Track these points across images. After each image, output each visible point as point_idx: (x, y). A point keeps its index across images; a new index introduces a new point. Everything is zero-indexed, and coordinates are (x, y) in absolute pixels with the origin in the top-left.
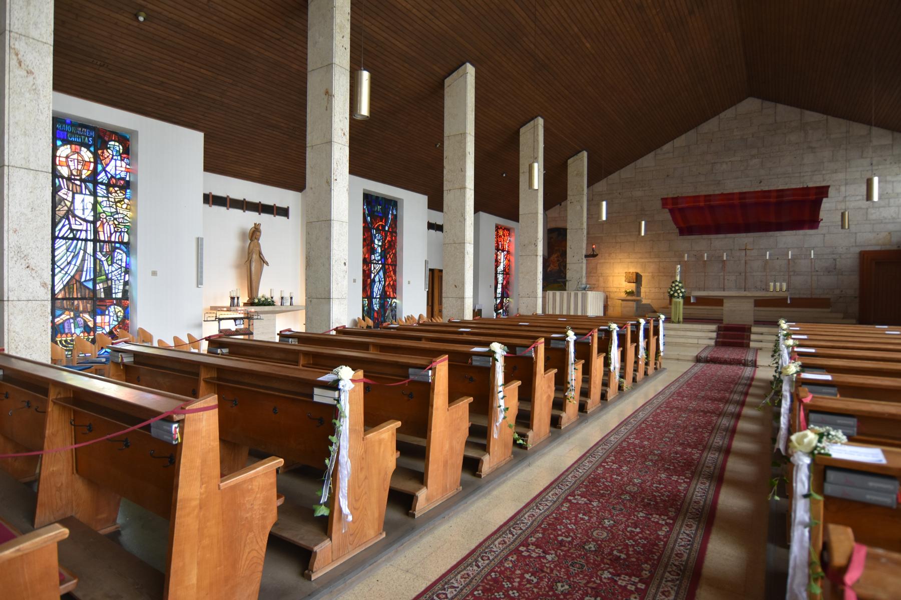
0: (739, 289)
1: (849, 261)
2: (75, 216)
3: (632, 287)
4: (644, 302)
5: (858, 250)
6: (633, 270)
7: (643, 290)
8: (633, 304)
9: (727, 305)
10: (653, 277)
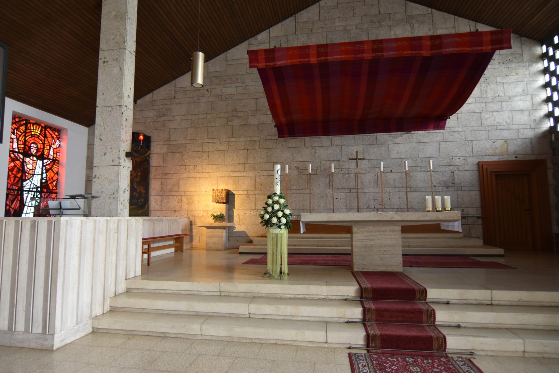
0: (349, 209)
1: (468, 174)
2: (52, 171)
3: (221, 209)
4: (238, 228)
5: (476, 161)
6: (223, 186)
7: (236, 213)
8: (224, 233)
9: (360, 237)
10: (248, 196)
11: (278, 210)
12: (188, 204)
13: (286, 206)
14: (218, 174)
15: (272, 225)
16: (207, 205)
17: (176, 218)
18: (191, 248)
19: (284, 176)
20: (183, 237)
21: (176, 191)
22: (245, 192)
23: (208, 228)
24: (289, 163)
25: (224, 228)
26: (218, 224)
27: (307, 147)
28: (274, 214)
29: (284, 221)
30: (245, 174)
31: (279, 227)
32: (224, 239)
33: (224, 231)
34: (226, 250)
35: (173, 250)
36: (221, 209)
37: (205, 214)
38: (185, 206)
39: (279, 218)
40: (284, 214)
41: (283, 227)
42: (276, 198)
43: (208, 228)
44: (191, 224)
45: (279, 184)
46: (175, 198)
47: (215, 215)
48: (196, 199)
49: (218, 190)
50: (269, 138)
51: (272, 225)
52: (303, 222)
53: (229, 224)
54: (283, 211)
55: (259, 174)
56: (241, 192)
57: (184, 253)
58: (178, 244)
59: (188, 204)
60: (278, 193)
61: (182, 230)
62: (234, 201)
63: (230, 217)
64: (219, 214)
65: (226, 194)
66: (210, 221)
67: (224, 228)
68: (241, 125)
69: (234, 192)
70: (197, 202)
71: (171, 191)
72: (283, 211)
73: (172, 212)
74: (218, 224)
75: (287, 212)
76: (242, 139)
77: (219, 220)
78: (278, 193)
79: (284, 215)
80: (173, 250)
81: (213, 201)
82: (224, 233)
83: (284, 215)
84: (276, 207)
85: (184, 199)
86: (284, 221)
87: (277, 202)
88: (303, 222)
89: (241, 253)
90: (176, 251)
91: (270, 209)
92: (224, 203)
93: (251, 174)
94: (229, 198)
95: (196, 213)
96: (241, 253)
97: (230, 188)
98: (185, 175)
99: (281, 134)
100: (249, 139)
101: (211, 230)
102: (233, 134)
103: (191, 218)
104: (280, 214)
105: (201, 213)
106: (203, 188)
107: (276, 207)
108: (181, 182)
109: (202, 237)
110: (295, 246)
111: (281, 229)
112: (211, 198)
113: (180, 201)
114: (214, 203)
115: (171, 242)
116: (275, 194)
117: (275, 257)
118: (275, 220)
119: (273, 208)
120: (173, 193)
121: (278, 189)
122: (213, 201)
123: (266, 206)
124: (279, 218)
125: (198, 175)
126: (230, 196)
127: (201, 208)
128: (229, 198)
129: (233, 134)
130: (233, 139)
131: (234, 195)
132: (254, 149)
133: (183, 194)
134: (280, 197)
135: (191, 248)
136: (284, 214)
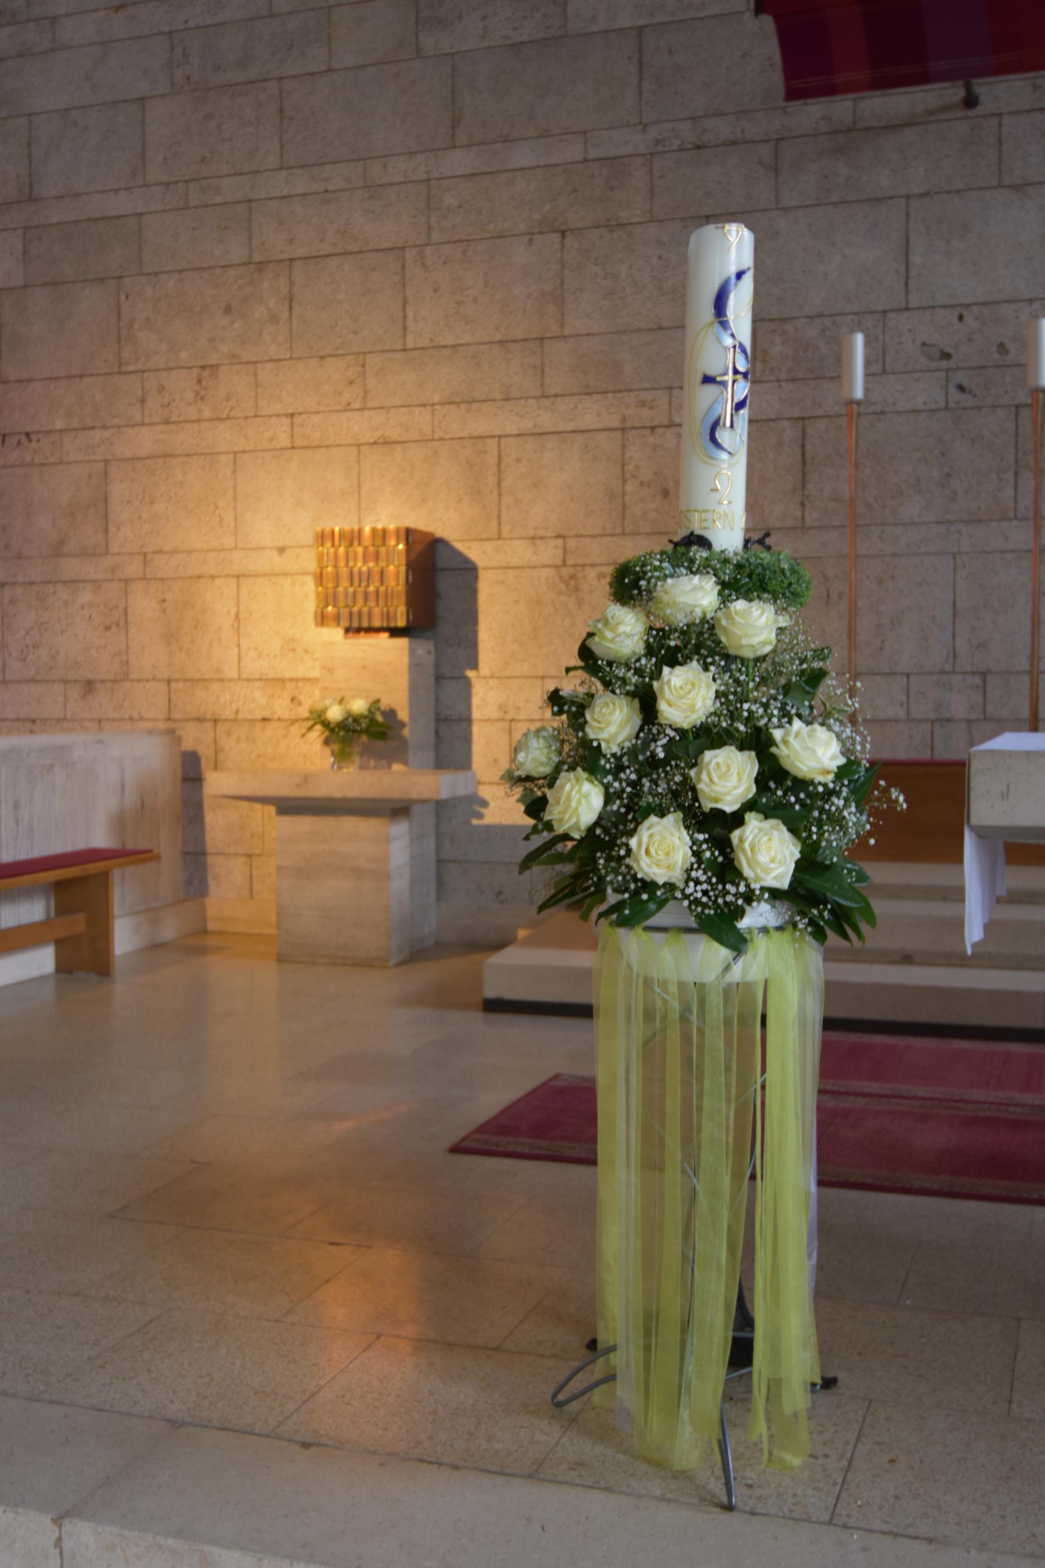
8: (397, 845)
11: (707, 736)
12: (170, 638)
13: (800, 685)
14: (361, 426)
15: (642, 900)
16: (291, 646)
17: (60, 739)
18: (199, 942)
19: (790, 350)
20: (104, 878)
21: (89, 554)
22: (550, 552)
23: (288, 807)
24: (877, 321)
25: (398, 810)
26: (355, 780)
27: (1019, 188)
28: (656, 773)
29: (770, 853)
30: (546, 420)
31: (721, 924)
32: (400, 885)
33: (400, 829)
34: (416, 954)
35: (41, 961)
36: (378, 670)
37: (282, 708)
38: (149, 654)
39: (716, 828)
40: (772, 774)
41: (758, 916)
42: (694, 595)
43: (288, 807)
44: (191, 772)
45: (736, 438)
46: (85, 596)
47: (335, 714)
48: (219, 600)
49: (353, 537)
50: (722, 129)
51: (642, 900)
52: (983, 834)
53: (440, 785)
54: (759, 743)
55: (645, 416)
56: (520, 552)
57: (122, 988)
58: (76, 924)
59: (170, 638)
60: (728, 534)
61: (119, 822)
62: (471, 617)
63: (448, 734)
64: (359, 706)
65: (412, 565)
66: (310, 761)
67: (398, 810)
68: (516, 47)
69: (474, 553)
70: (227, 622)
71: (58, 550)
72: (759, 743)
73: (75, 693)
74: (355, 780)
75: (815, 751)
76: (523, 156)
77: (366, 752)
78: (728, 534)
79: (779, 790)
80: (41, 961)
81: (322, 619)
82: (397, 845)
83: (779, 790)
84: (689, 695)
85: (143, 605)
86: (770, 853)
87: (700, 643)
88: (983, 834)
89: (495, 1006)
90: (64, 967)
91: (613, 723)
92: (395, 632)
93: (591, 413)
94: (433, 595)
95: (225, 701)
96: (495, 1006)
97: (445, 521)
98: (144, 440)
99: (808, 71)
100: (573, 152)
101: (305, 823)
102: (456, 122)
103: (192, 738)
104: (727, 777)
105: (256, 701)
106: (263, 530)
107: (689, 695)
108: (118, 490)
109: (257, 866)
110: (907, 959)
111: (738, 943)
112: (306, 595)
113: (119, 622)
114: (335, 634)
115: (32, 911)
116: (689, 549)
117: (673, 1245)
118: (663, 849)
119: (647, 703)
120: (72, 567)
121: (724, 503)
122: (322, 619)
123: (572, 686)
124: (716, 828)
125: (225, 437)
126: (444, 584)
127: (254, 666)
128: (433, 595)
129: (456, 122)
130: (459, 162)
131: (469, 570)
132: (611, 226)
133: (134, 568)
134: (743, 580)
135: (199, 942)
136: (772, 774)
